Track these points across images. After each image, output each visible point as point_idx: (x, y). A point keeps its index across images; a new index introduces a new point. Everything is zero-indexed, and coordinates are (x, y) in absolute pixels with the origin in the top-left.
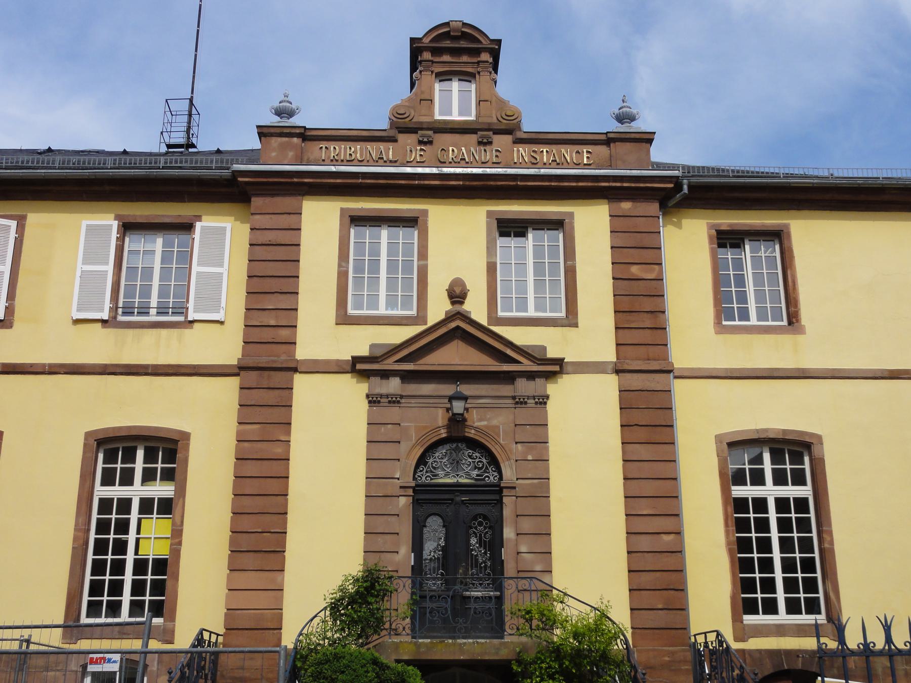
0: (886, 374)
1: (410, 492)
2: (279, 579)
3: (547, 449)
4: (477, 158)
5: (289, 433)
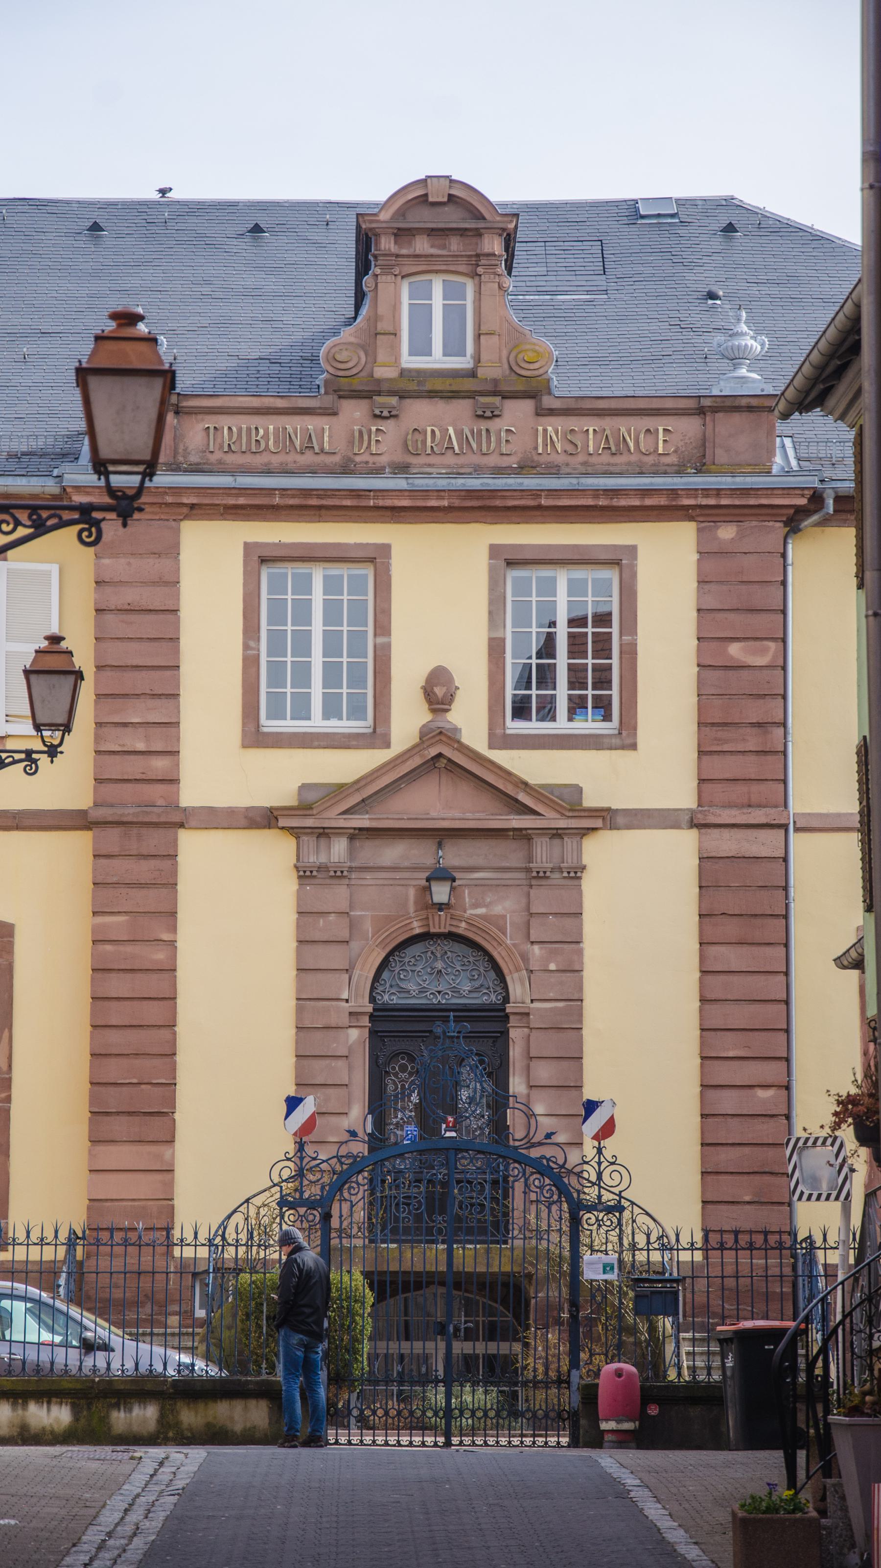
1: (366, 1021)
2: (168, 1154)
3: (580, 953)
4: (474, 446)
5: (174, 929)
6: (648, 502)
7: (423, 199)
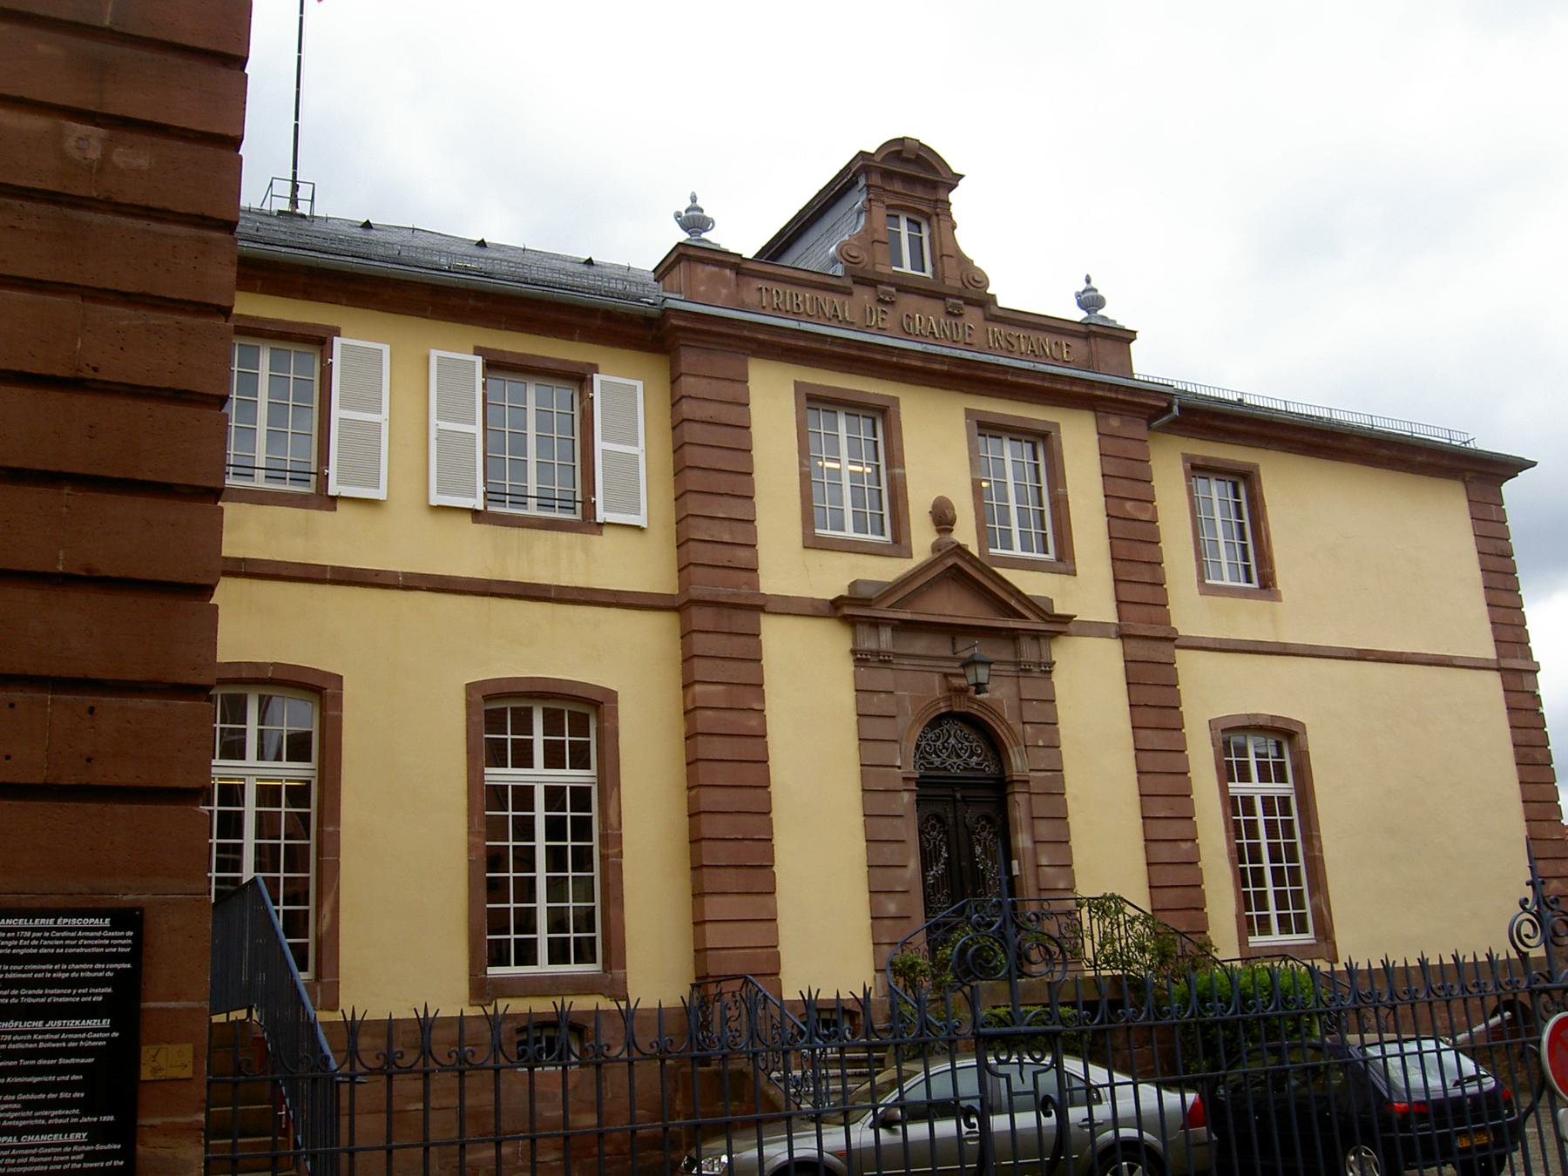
0: (1354, 655)
5: (762, 699)
6: (1075, 389)
7: (899, 153)
